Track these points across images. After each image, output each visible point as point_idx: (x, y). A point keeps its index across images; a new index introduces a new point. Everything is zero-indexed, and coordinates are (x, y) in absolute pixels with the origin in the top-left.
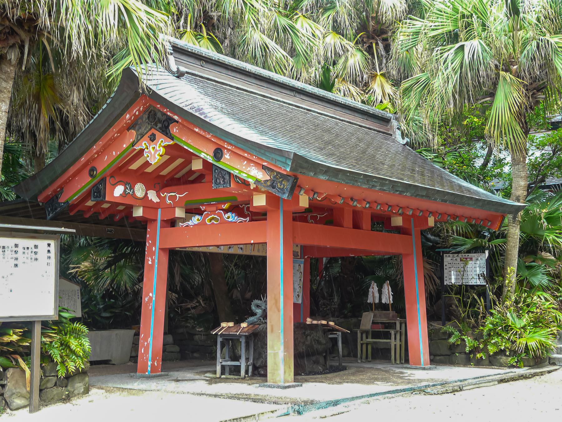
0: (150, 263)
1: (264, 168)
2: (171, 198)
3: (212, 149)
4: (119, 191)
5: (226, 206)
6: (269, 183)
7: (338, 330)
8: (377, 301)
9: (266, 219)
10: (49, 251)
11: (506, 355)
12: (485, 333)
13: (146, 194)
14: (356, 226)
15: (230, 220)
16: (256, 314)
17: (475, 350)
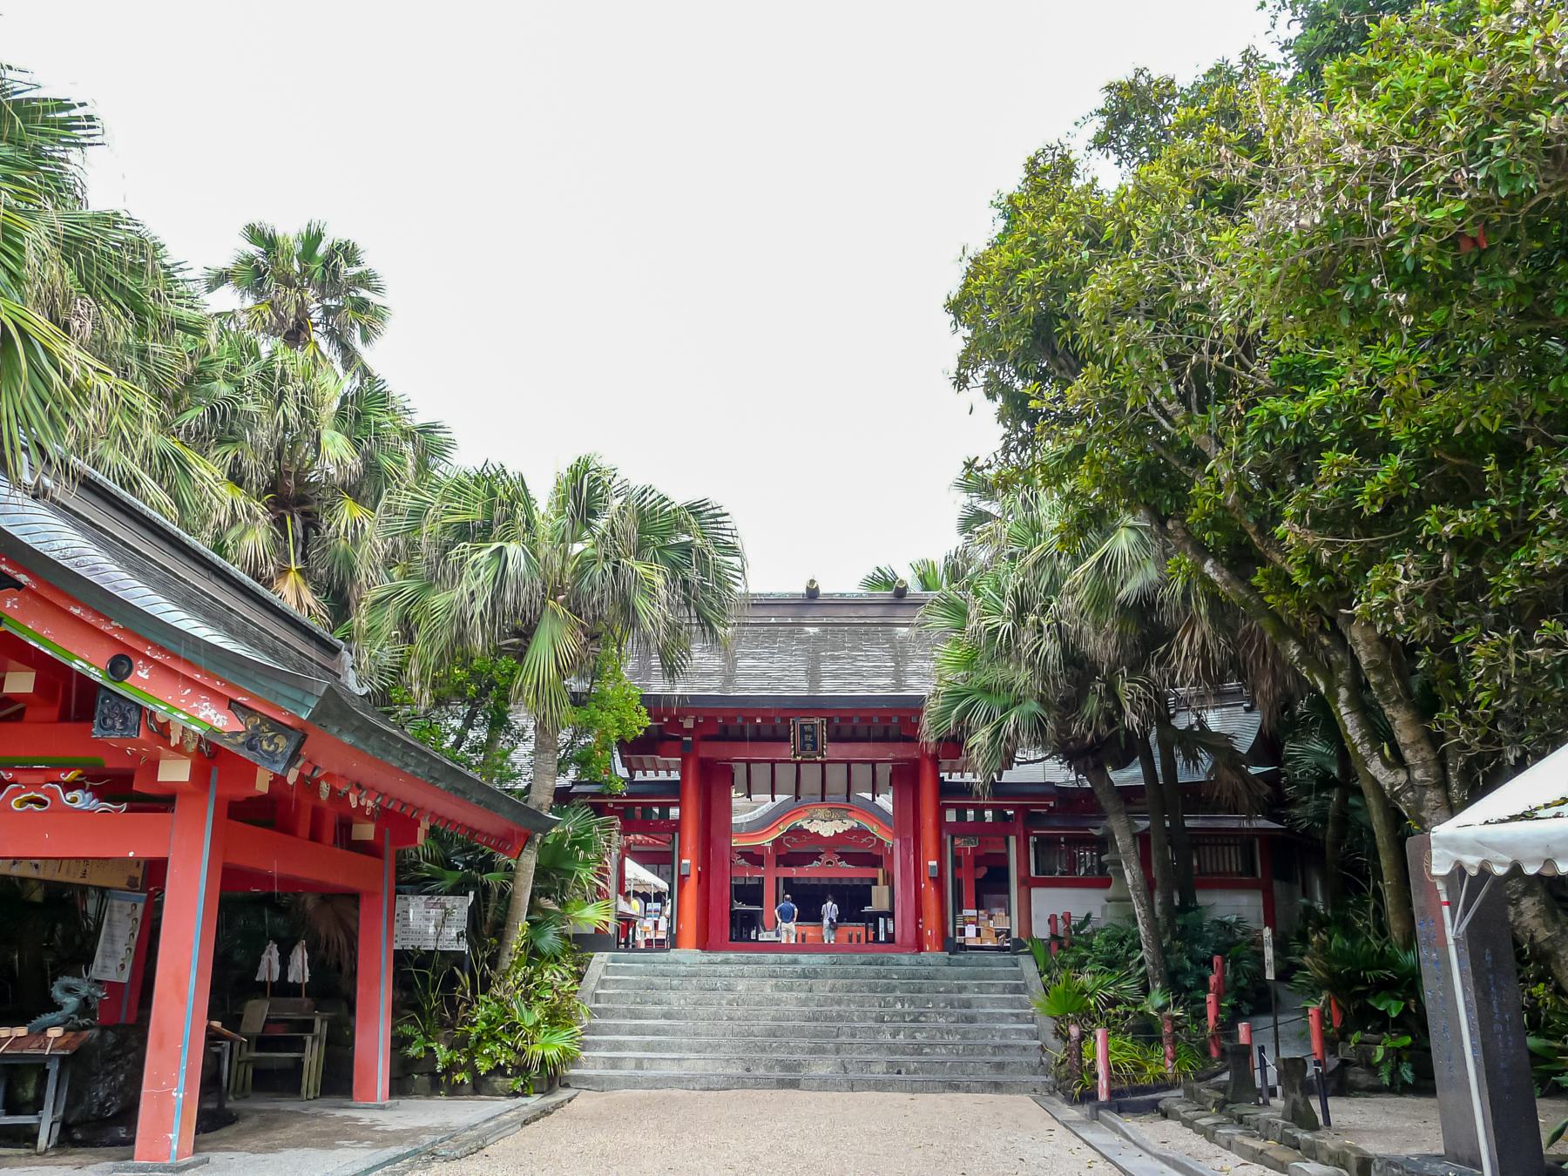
1: (233, 705)
3: (105, 654)
5: (71, 775)
6: (240, 739)
7: (225, 1038)
8: (276, 978)
11: (505, 1075)
12: (473, 1037)
14: (315, 836)
15: (76, 805)
16: (60, 1008)
17: (452, 1068)
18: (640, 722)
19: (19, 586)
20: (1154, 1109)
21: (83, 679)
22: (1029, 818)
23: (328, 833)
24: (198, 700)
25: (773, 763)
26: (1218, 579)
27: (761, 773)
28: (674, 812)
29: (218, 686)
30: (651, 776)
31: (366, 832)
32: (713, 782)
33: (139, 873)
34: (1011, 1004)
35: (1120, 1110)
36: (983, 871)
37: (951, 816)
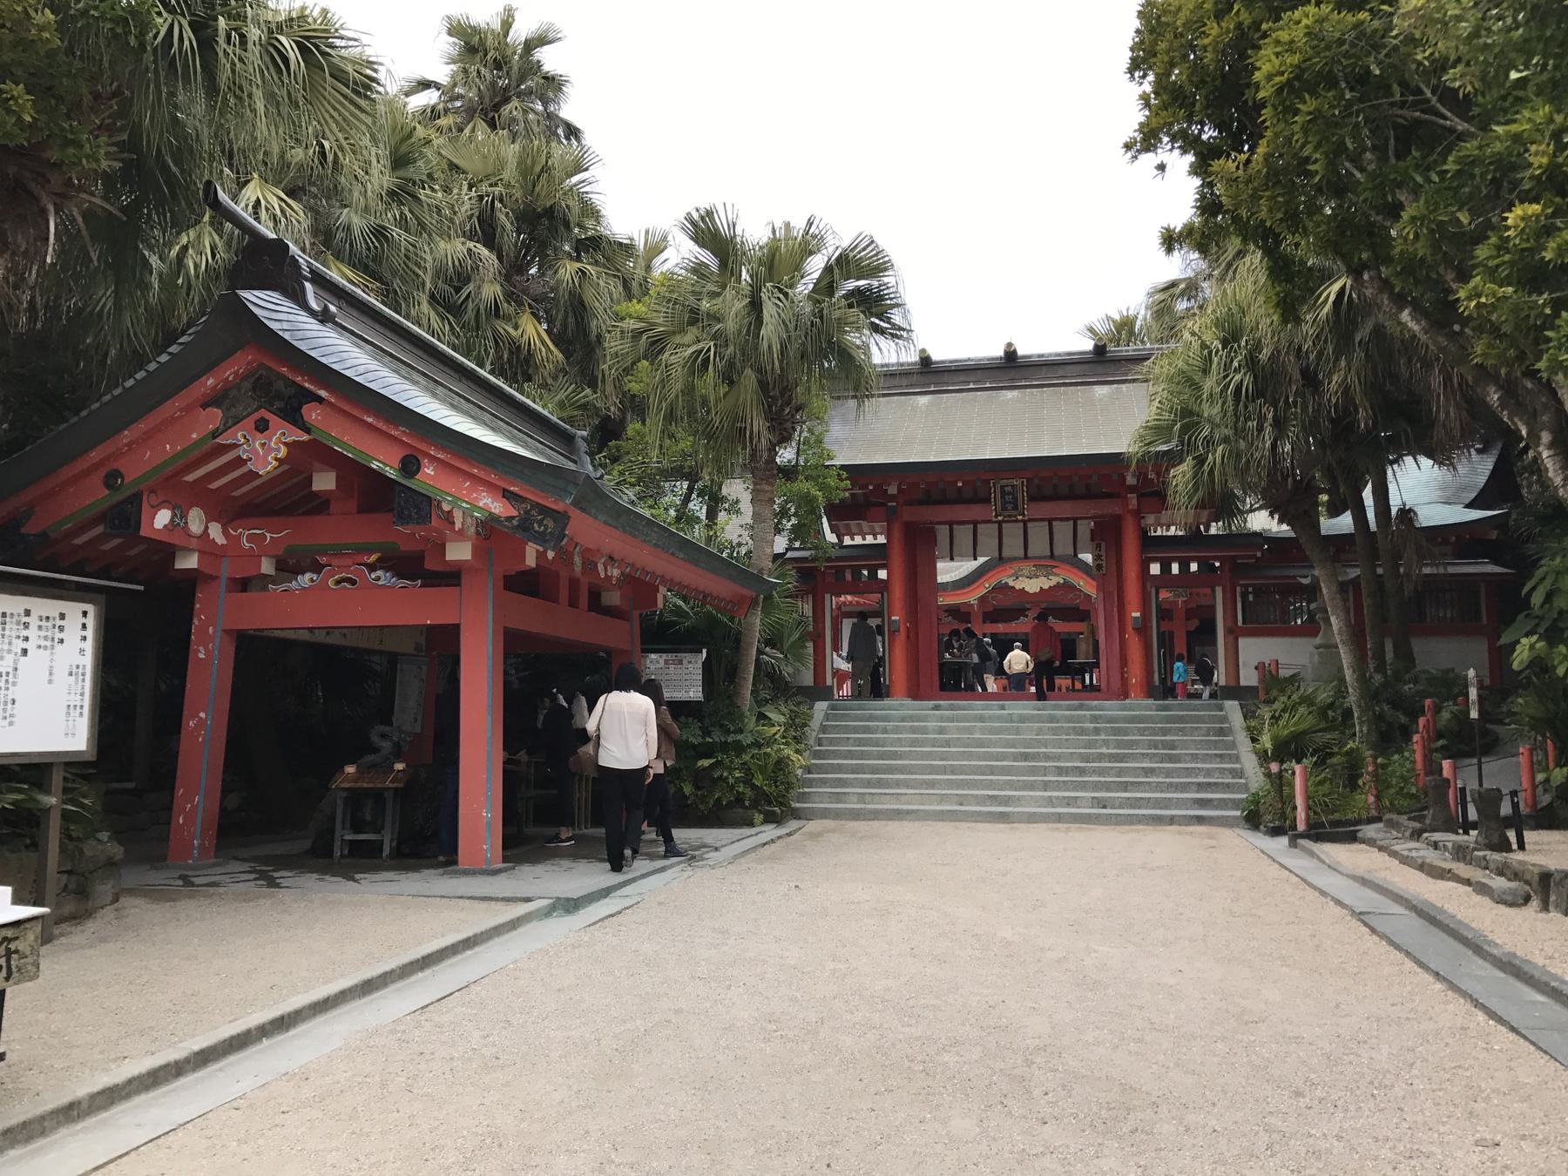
0: (201, 656)
1: (507, 495)
2: (250, 538)
4: (163, 518)
5: (373, 558)
6: (515, 522)
9: (459, 585)
10: (84, 626)
13: (207, 528)
14: (573, 603)
18: (843, 490)
19: (320, 400)
20: (1352, 838)
21: (379, 476)
22: (1236, 568)
23: (584, 601)
24: (476, 491)
25: (975, 523)
26: (1416, 328)
27: (964, 534)
28: (882, 574)
29: (492, 478)
30: (858, 540)
31: (613, 598)
32: (919, 547)
33: (423, 640)
34: (1215, 745)
35: (1318, 838)
36: (1194, 624)
37: (1155, 569)
